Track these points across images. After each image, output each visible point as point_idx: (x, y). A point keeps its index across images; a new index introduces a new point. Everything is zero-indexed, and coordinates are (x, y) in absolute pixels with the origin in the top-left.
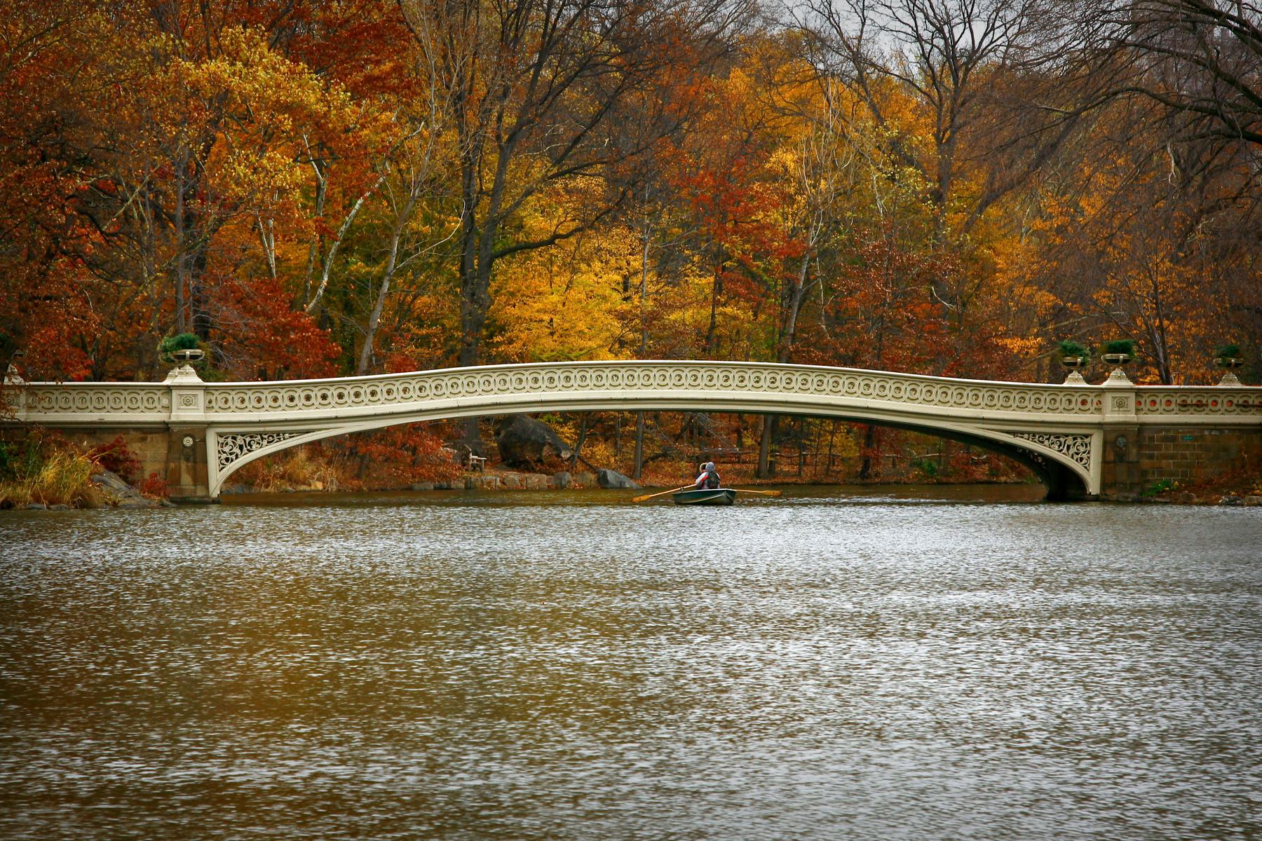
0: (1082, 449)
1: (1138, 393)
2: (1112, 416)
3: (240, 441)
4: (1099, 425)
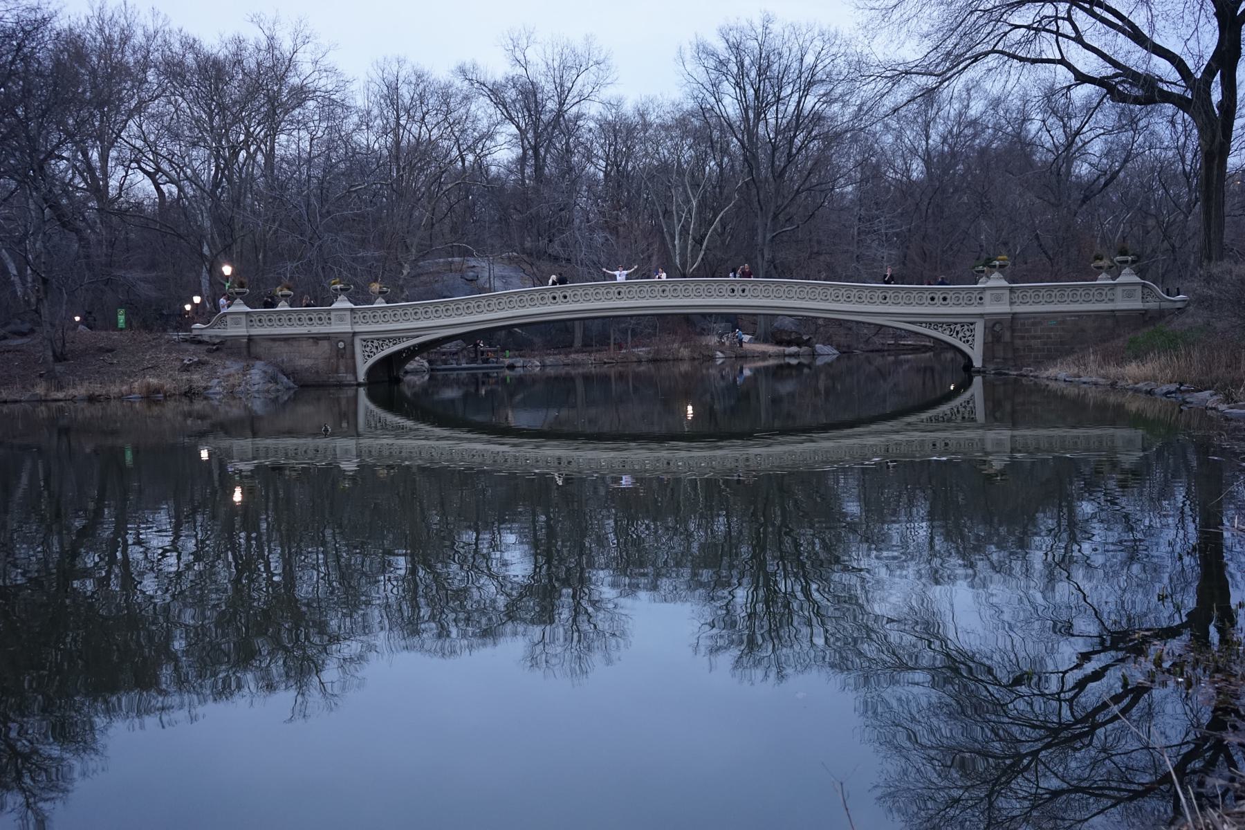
0: (968, 334)
1: (1012, 290)
2: (990, 308)
3: (376, 344)
4: (981, 315)
